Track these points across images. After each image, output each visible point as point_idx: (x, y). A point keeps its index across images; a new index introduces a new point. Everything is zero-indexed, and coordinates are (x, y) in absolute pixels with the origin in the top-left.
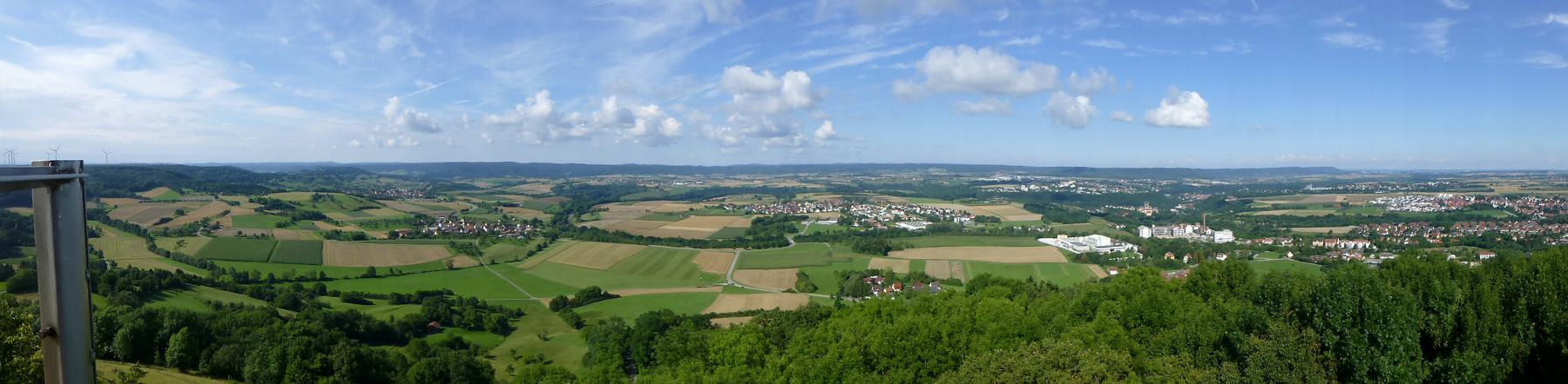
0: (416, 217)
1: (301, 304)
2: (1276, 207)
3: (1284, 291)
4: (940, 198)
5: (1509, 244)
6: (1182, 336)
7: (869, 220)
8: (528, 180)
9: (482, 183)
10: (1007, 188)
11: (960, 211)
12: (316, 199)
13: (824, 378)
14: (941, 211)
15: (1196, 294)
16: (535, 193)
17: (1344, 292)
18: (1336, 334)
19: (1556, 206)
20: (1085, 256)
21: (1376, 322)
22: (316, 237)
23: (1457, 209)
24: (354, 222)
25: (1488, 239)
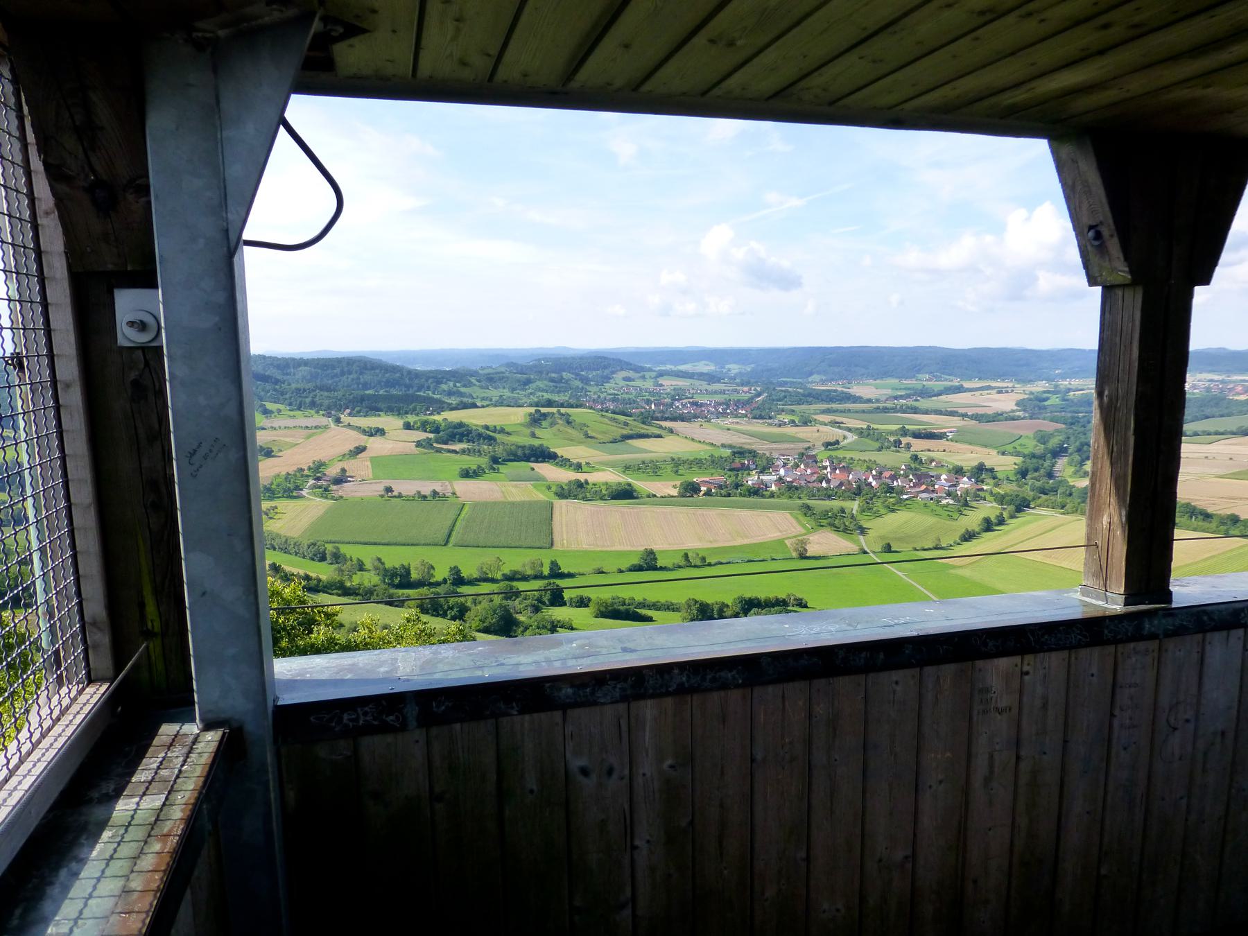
0: (734, 453)
1: (517, 623)
8: (967, 385)
9: (865, 390)
12: (536, 420)
16: (981, 411)
22: (541, 496)
24: (613, 465)
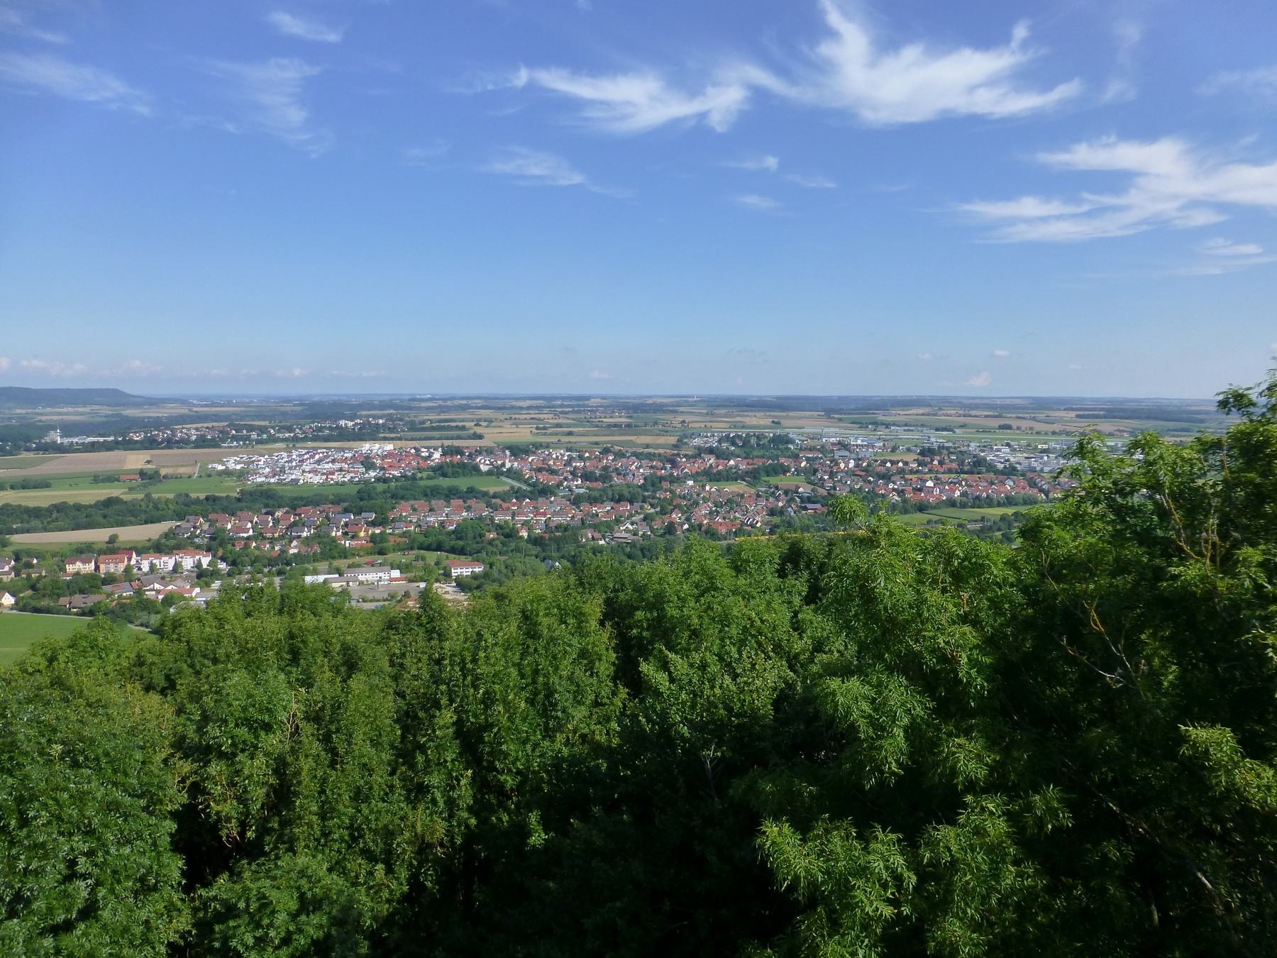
5: (513, 545)
19: (605, 468)
23: (404, 476)
25: (470, 535)
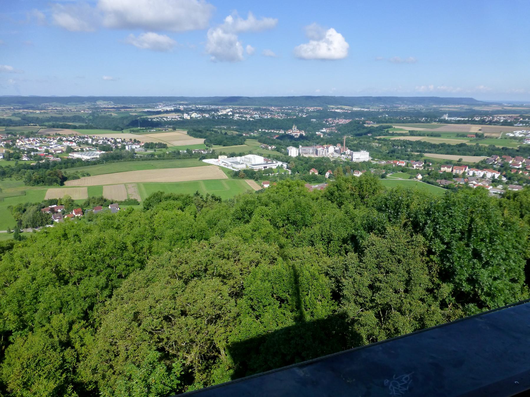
2: (412, 133)
3: (404, 203)
4: (110, 129)
6: (318, 233)
7: (38, 153)
10: (170, 117)
11: (131, 140)
13: (19, 301)
14: (113, 141)
15: (332, 202)
17: (457, 212)
18: (443, 243)
20: (242, 173)
21: (482, 240)
